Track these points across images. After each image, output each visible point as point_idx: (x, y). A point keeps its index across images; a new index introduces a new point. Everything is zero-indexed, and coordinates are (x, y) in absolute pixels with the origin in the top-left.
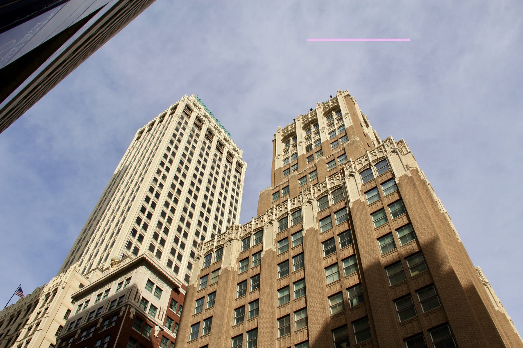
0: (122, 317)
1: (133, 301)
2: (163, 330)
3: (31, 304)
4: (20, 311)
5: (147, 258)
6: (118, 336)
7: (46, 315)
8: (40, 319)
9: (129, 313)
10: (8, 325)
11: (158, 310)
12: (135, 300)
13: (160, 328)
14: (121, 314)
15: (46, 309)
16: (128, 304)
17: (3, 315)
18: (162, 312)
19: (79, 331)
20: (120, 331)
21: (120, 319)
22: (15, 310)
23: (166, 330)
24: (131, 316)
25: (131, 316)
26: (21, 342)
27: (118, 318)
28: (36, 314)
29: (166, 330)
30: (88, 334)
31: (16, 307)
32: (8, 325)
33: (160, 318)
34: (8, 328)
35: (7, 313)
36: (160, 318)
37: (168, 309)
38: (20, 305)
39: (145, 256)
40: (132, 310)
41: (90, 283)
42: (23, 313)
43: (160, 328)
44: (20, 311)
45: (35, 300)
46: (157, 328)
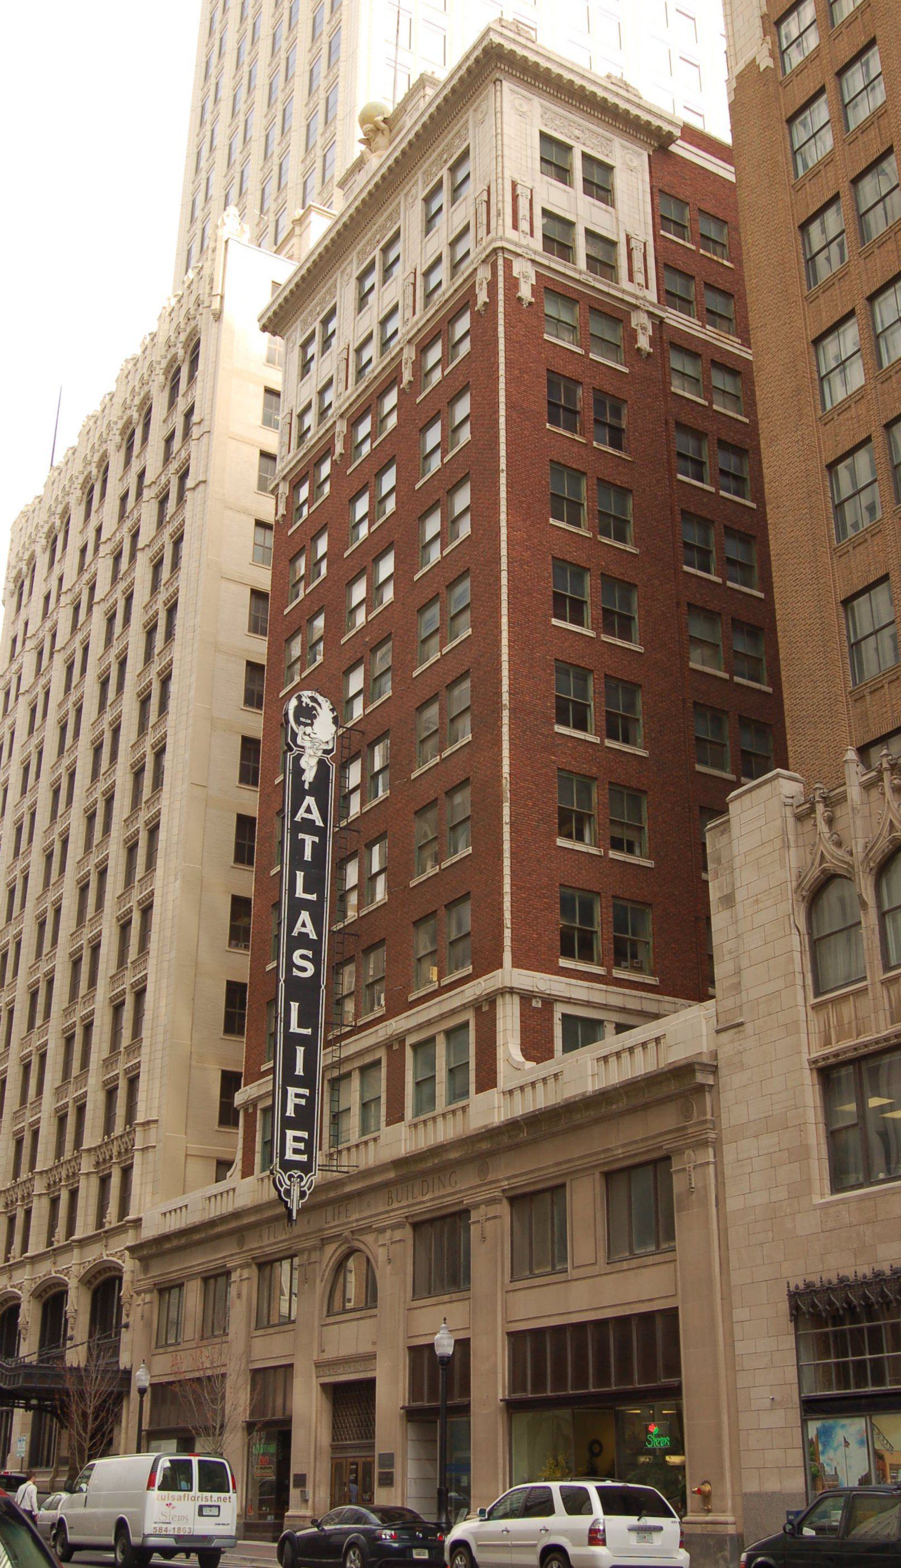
0: (491, 305)
1: (510, 234)
2: (661, 320)
3: (88, 477)
4: (66, 510)
5: (508, 46)
6: (502, 380)
7: (195, 432)
8: (183, 454)
9: (512, 284)
10: (128, 462)
11: (622, 250)
12: (515, 227)
13: (650, 314)
14: (482, 297)
15: (189, 413)
16: (495, 250)
17: (25, 539)
18: (638, 256)
19: (342, 427)
20: (502, 360)
21: (484, 320)
22: (87, 463)
23: (675, 318)
24: (525, 292)
25: (525, 292)
26: (156, 548)
27: (476, 317)
28: (77, 554)
29: (675, 318)
30: (379, 423)
31: (85, 451)
32: (128, 462)
33: (640, 278)
34: (94, 522)
35: (31, 529)
36: (640, 278)
37: (656, 235)
38: (95, 438)
39: (497, 40)
40: (519, 267)
41: (298, 265)
42: (42, 561)
43: (650, 314)
44: (66, 510)
45: (96, 458)
46: (639, 320)
